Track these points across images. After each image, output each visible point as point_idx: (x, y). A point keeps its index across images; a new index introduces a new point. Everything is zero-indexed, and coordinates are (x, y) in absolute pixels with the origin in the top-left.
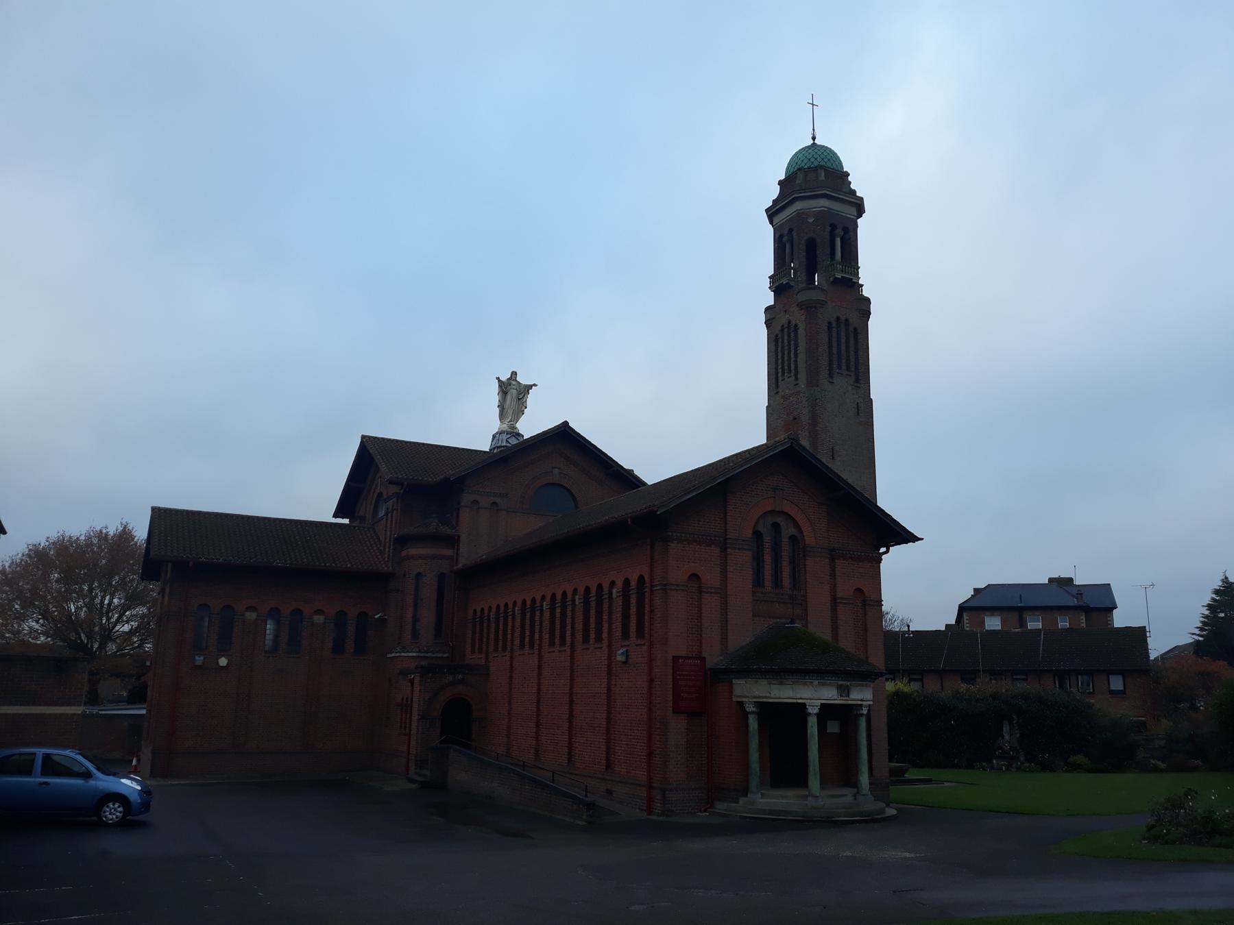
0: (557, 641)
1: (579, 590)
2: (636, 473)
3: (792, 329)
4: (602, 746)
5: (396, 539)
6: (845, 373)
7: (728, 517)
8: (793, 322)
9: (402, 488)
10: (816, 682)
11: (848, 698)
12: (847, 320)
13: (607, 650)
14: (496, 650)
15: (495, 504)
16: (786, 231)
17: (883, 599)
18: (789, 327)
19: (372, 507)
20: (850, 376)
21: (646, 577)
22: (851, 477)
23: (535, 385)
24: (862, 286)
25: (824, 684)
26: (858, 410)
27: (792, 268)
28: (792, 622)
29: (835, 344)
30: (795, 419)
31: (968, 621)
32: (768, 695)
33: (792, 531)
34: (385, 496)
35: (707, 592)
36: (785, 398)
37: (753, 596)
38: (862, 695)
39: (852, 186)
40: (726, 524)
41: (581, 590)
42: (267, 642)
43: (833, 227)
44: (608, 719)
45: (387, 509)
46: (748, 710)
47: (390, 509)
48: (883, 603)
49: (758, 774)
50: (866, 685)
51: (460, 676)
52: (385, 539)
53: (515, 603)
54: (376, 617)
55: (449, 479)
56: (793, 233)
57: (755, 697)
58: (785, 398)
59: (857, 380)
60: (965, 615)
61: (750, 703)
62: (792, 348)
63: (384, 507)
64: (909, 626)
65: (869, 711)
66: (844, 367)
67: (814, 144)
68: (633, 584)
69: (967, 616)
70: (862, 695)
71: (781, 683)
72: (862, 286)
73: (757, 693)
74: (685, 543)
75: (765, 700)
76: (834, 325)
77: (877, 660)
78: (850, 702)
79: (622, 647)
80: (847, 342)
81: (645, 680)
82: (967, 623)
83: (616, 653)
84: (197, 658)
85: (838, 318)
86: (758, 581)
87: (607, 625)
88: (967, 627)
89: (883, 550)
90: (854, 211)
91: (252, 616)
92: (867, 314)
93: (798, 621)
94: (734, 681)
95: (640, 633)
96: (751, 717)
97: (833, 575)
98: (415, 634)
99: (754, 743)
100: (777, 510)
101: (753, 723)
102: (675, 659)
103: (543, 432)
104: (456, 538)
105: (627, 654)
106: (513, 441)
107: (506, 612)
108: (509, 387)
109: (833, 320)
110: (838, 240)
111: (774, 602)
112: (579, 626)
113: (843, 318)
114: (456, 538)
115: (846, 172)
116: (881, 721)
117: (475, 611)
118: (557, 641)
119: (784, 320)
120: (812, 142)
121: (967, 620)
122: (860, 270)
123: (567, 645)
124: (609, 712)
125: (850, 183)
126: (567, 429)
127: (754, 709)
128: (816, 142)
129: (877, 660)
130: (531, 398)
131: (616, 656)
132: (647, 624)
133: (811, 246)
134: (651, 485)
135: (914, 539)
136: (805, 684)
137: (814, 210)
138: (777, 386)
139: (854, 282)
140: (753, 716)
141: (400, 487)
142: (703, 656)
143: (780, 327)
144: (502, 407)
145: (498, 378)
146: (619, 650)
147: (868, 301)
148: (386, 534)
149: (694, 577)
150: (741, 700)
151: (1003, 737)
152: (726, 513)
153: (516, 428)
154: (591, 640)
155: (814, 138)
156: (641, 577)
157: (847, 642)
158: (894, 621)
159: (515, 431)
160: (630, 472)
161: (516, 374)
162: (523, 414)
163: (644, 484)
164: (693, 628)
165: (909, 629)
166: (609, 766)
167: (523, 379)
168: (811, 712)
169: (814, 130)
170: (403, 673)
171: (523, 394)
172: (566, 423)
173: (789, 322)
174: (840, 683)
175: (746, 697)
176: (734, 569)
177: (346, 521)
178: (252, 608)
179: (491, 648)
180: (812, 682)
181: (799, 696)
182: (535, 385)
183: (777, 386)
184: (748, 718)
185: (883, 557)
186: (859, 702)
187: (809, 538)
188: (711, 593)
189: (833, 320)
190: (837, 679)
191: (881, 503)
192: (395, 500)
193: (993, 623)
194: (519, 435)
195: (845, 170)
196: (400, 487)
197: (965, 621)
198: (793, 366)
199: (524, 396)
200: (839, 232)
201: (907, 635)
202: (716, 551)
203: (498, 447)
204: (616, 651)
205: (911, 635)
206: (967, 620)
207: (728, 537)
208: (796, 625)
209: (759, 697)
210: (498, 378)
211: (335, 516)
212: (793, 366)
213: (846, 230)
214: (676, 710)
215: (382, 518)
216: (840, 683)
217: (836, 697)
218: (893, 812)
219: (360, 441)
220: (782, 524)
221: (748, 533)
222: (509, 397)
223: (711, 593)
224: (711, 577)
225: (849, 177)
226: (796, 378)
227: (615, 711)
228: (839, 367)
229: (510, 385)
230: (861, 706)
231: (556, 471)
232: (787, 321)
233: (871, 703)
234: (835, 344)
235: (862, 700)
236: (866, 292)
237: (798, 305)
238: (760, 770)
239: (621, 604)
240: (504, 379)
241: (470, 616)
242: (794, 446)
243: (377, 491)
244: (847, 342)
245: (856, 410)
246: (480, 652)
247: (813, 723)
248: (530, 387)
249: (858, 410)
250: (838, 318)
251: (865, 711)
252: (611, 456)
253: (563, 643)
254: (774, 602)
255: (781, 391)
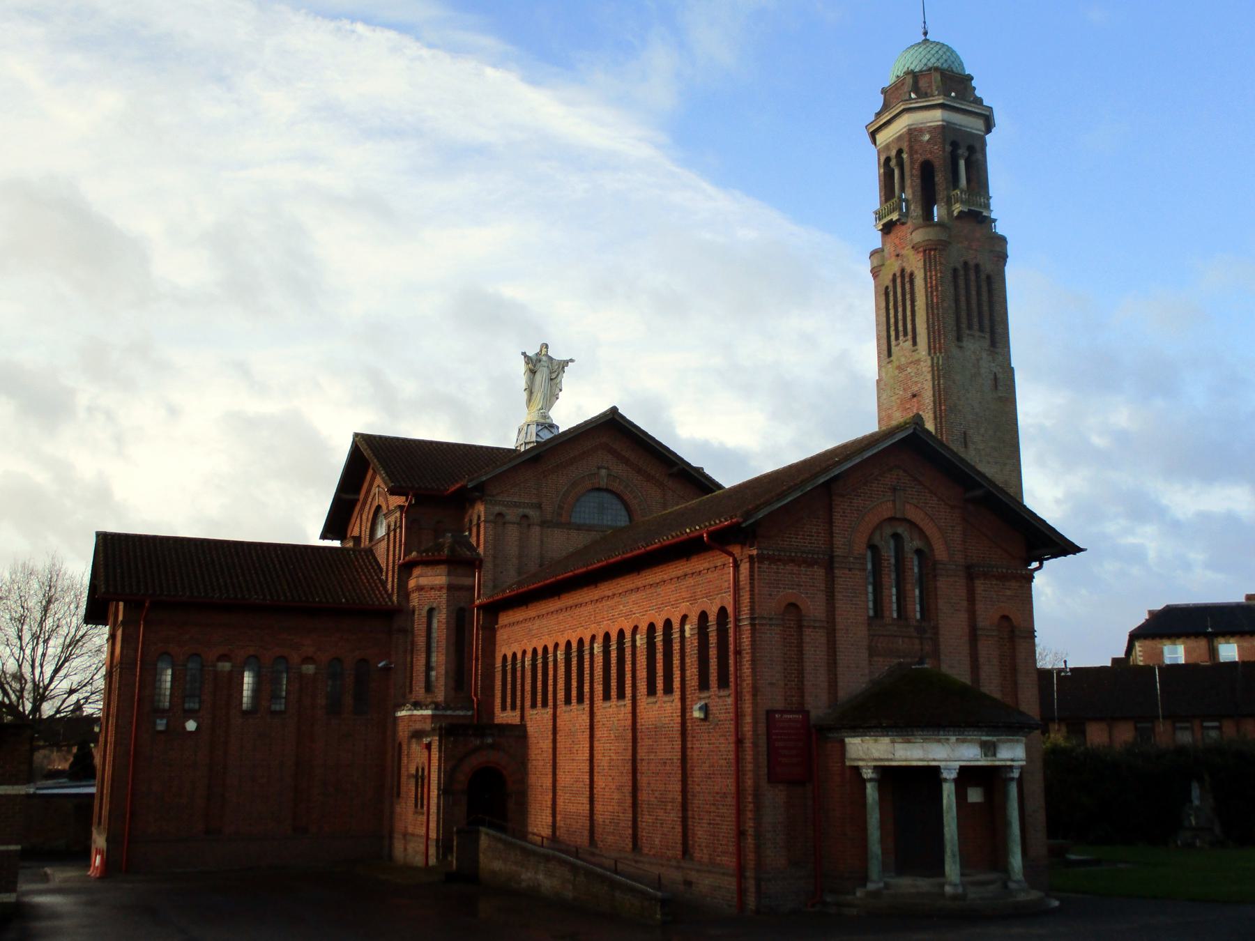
0: (614, 693)
1: (640, 627)
2: (707, 471)
3: (905, 278)
4: (676, 827)
5: (401, 566)
6: (977, 334)
7: (834, 528)
8: (908, 270)
9: (407, 500)
10: (953, 739)
11: (994, 758)
12: (977, 266)
13: (679, 704)
14: (534, 705)
15: (525, 517)
16: (893, 153)
17: (1036, 629)
18: (903, 276)
19: (369, 525)
20: (984, 337)
21: (730, 610)
22: (988, 469)
23: (572, 360)
24: (994, 221)
25: (964, 741)
26: (996, 383)
27: (904, 200)
28: (921, 662)
29: (963, 299)
30: (914, 396)
31: (1141, 654)
32: (890, 756)
33: (917, 543)
34: (384, 510)
35: (809, 627)
36: (900, 368)
37: (869, 630)
38: (1012, 753)
39: (978, 93)
40: (832, 537)
41: (643, 627)
42: (245, 700)
43: (955, 145)
44: (684, 791)
45: (389, 527)
46: (865, 776)
47: (392, 527)
48: (1036, 634)
49: (880, 857)
50: (1017, 741)
51: (490, 740)
52: (387, 565)
53: (556, 645)
54: (380, 665)
55: (869, 618)
56: (903, 155)
57: (875, 760)
58: (900, 368)
59: (993, 344)
60: (1137, 644)
61: (868, 767)
62: (908, 303)
63: (384, 525)
64: (1065, 662)
65: (1021, 774)
66: (976, 326)
67: (926, 40)
68: (712, 618)
69: (1140, 646)
70: (1012, 753)
71: (909, 742)
72: (994, 221)
73: (876, 755)
74: (779, 563)
75: (886, 763)
76: (962, 272)
77: (1029, 703)
78: (997, 763)
79: (700, 699)
80: (979, 294)
81: (731, 741)
82: (1140, 656)
83: (692, 708)
84: (158, 721)
85: (966, 263)
86: (416, 806)
87: (679, 672)
88: (1141, 661)
89: (1035, 565)
90: (979, 124)
91: (226, 666)
92: (1003, 257)
93: (927, 660)
94: (847, 740)
95: (723, 683)
96: (869, 786)
97: (971, 598)
98: (428, 687)
99: (874, 818)
100: (898, 516)
101: (871, 791)
102: (770, 713)
103: (586, 422)
104: (477, 563)
105: (705, 709)
106: (546, 435)
107: (668, 641)
108: (538, 365)
109: (959, 266)
110: (962, 163)
111: (896, 636)
112: (642, 674)
113: (972, 263)
114: (477, 563)
115: (969, 75)
116: (1036, 786)
117: (505, 657)
118: (614, 693)
119: (893, 266)
120: (924, 38)
121: (1140, 651)
122: (991, 201)
123: (627, 699)
124: (684, 781)
125: (974, 88)
126: (616, 417)
127: (874, 776)
128: (928, 37)
129: (1029, 703)
130: (567, 379)
131: (692, 712)
132: (732, 669)
133: (927, 171)
134: (730, 489)
135: (1075, 549)
136: (939, 741)
137: (928, 125)
138: (890, 354)
139: (985, 216)
140: (873, 783)
141: (404, 498)
142: (806, 709)
143: (891, 277)
144: (530, 391)
145: (524, 354)
146: (696, 704)
147: (1003, 240)
148: (388, 559)
149: (793, 606)
150: (856, 764)
151: (1191, 801)
152: (830, 522)
153: (549, 418)
154: (658, 692)
155: (925, 34)
156: (723, 610)
157: (991, 686)
158: (1046, 656)
159: (548, 421)
160: (699, 471)
161: (547, 346)
162: (557, 398)
163: (719, 487)
164: (792, 673)
165: (1066, 665)
166: (686, 851)
167: (557, 354)
168: (948, 777)
169: (925, 23)
170: (417, 735)
171: (556, 373)
172: (614, 410)
173: (903, 270)
174: (984, 738)
175: (863, 760)
176: (844, 596)
177: (336, 544)
178: (224, 657)
179: (528, 703)
180: (948, 739)
181: (931, 757)
182: (572, 360)
183: (890, 354)
184: (865, 788)
185: (1036, 574)
186: (1009, 763)
187: (940, 552)
188: (815, 627)
189: (959, 266)
190: (980, 733)
191: (1030, 502)
192: (398, 514)
193: (1176, 653)
194: (551, 426)
195: (967, 73)
196: (404, 498)
197: (1139, 653)
198: (909, 326)
199: (558, 375)
200: (962, 151)
201: (1063, 674)
202: (819, 572)
203: (526, 443)
204: (692, 705)
205: (1069, 674)
206: (1140, 651)
207: (835, 554)
208: (926, 666)
209: (882, 760)
210: (524, 354)
211: (323, 537)
212: (909, 326)
213: (971, 149)
214: (773, 779)
215: (382, 539)
216: (984, 738)
217: (979, 757)
218: (1056, 903)
219: (352, 440)
220: (906, 535)
221: (860, 546)
222: (538, 376)
223: (815, 627)
224: (814, 607)
225: (973, 82)
226: (915, 343)
227: (693, 781)
228: (970, 327)
229: (540, 361)
230: (1011, 767)
231: (603, 472)
232: (900, 269)
233: (1024, 763)
234: (963, 299)
235: (1012, 760)
236: (1000, 229)
237: (913, 247)
238: (883, 854)
239: (697, 644)
240: (531, 353)
241: (499, 664)
242: (917, 432)
243: (376, 504)
244: (979, 294)
245: (994, 383)
246: (514, 708)
247: (948, 791)
248: (566, 363)
249: (996, 383)
250: (966, 263)
251: (1016, 774)
252: (690, 462)
253: (621, 695)
254: (896, 636)
255: (894, 360)
